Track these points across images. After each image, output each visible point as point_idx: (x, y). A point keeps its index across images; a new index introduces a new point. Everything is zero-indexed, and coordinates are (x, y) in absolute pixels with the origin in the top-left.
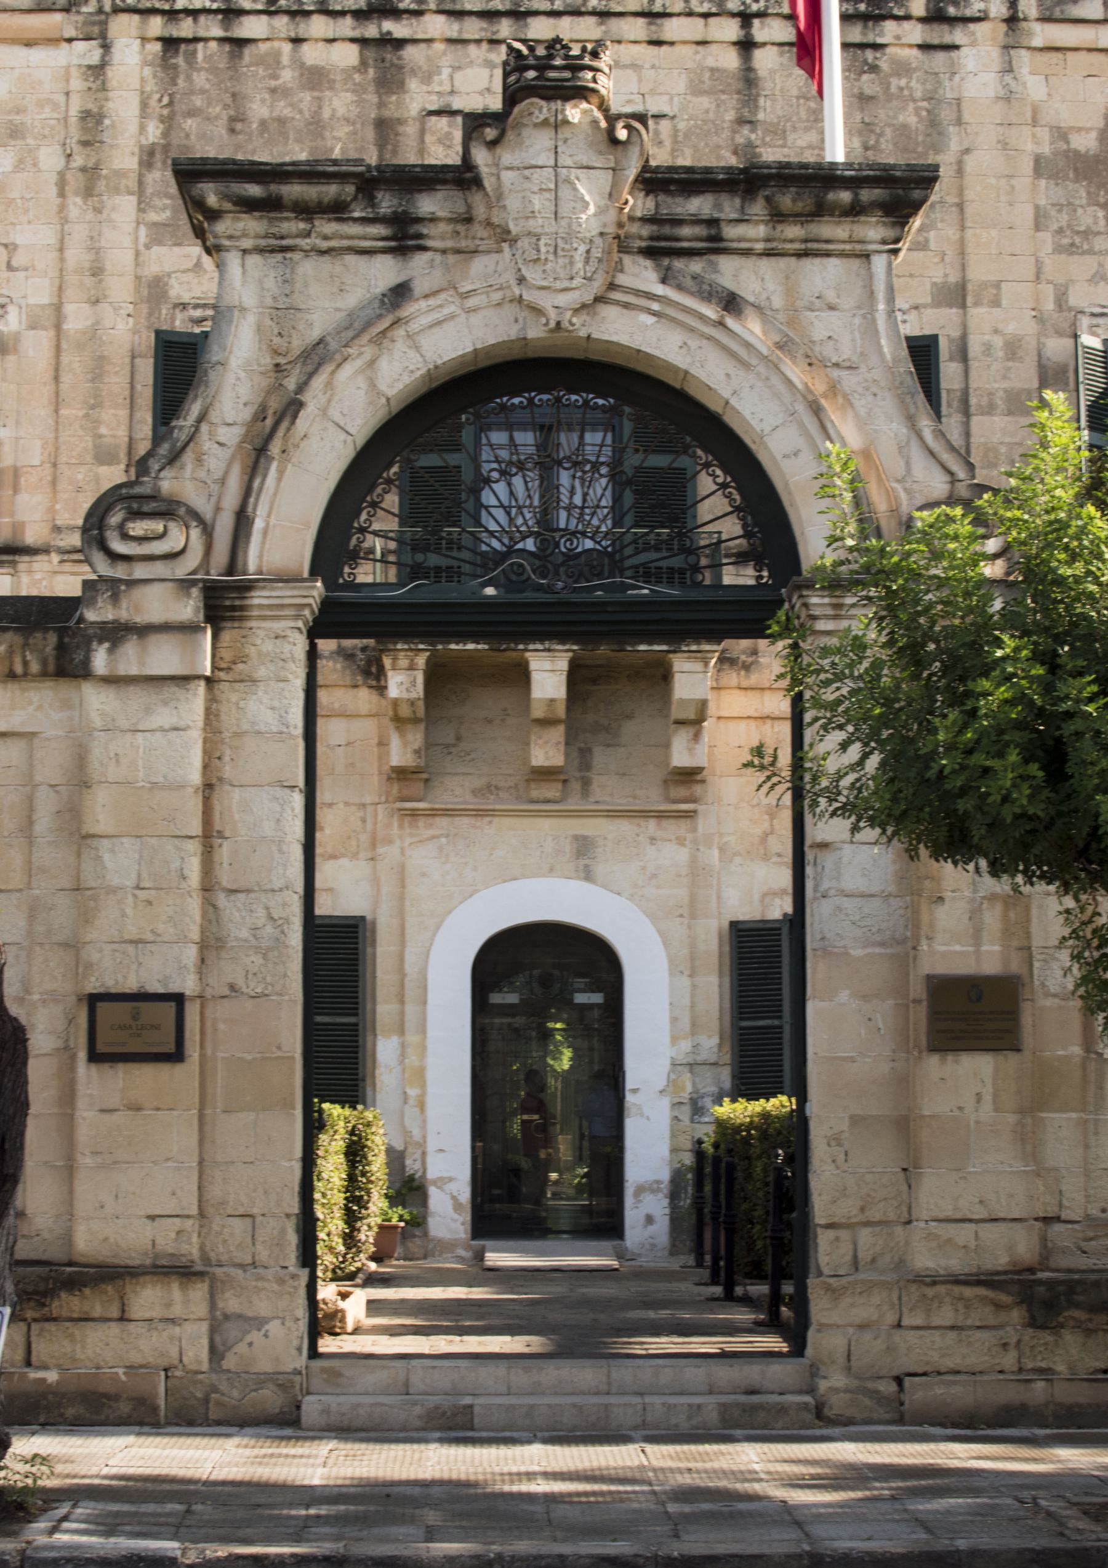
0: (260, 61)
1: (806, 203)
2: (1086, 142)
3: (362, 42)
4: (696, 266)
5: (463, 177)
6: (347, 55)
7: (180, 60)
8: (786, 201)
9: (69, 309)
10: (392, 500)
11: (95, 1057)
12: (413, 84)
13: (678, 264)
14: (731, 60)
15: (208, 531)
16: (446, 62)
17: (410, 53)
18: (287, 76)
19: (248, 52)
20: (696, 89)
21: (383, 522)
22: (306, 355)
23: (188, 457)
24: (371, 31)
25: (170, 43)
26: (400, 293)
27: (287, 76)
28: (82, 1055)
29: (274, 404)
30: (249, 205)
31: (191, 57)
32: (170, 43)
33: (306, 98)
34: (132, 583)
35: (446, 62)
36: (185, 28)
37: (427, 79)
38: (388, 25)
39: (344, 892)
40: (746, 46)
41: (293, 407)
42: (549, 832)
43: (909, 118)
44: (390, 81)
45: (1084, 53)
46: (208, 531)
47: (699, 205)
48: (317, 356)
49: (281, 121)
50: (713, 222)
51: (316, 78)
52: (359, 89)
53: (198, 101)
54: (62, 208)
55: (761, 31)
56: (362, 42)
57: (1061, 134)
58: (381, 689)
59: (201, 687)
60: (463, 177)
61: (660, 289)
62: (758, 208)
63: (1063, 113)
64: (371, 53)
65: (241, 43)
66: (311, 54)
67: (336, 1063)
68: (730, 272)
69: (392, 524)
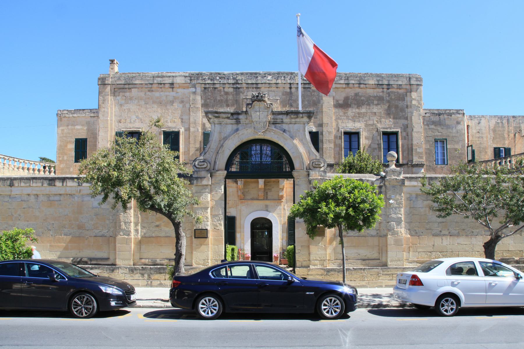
0: (218, 91)
1: (295, 116)
2: (341, 102)
3: (234, 88)
4: (280, 125)
5: (246, 112)
6: (231, 90)
7: (207, 91)
8: (292, 116)
9: (191, 128)
10: (239, 156)
11: (195, 237)
12: (241, 94)
13: (277, 125)
14: (288, 90)
15: (210, 164)
16: (246, 91)
17: (241, 89)
18: (222, 93)
19: (216, 90)
20: (283, 95)
21: (237, 159)
22: (224, 139)
23: (207, 153)
24: (235, 86)
25: (205, 88)
26: (237, 130)
27: (222, 93)
28: (193, 237)
29: (219, 146)
30: (216, 117)
31: (208, 90)
32: (205, 88)
33: (225, 96)
34: (199, 171)
35: (246, 91)
36: (207, 86)
37: (243, 94)
38: (237, 85)
39: (231, 212)
40: (290, 88)
41: (222, 146)
42: (261, 203)
43: (314, 99)
44: (238, 94)
45: (143, 298)
46: (210, 164)
47: (280, 117)
48: (226, 139)
49: (222, 100)
50: (282, 119)
51: (227, 93)
52: (233, 95)
53: (209, 97)
54: (189, 113)
55: (292, 86)
56: (234, 88)
57: (337, 101)
58: (237, 184)
59: (209, 187)
60: (246, 112)
61: (274, 129)
62: (289, 117)
63: (338, 98)
64: (235, 90)
65: (215, 88)
66: (226, 90)
67: (230, 237)
68: (285, 126)
69: (238, 160)
